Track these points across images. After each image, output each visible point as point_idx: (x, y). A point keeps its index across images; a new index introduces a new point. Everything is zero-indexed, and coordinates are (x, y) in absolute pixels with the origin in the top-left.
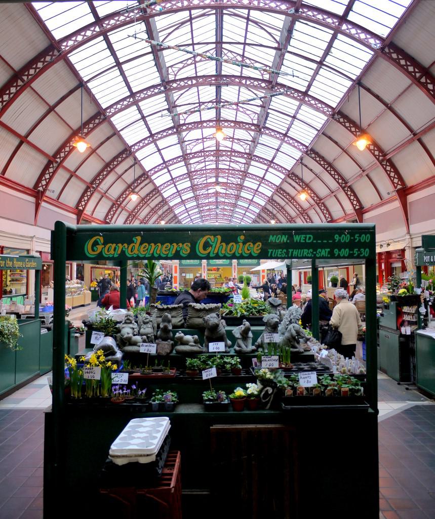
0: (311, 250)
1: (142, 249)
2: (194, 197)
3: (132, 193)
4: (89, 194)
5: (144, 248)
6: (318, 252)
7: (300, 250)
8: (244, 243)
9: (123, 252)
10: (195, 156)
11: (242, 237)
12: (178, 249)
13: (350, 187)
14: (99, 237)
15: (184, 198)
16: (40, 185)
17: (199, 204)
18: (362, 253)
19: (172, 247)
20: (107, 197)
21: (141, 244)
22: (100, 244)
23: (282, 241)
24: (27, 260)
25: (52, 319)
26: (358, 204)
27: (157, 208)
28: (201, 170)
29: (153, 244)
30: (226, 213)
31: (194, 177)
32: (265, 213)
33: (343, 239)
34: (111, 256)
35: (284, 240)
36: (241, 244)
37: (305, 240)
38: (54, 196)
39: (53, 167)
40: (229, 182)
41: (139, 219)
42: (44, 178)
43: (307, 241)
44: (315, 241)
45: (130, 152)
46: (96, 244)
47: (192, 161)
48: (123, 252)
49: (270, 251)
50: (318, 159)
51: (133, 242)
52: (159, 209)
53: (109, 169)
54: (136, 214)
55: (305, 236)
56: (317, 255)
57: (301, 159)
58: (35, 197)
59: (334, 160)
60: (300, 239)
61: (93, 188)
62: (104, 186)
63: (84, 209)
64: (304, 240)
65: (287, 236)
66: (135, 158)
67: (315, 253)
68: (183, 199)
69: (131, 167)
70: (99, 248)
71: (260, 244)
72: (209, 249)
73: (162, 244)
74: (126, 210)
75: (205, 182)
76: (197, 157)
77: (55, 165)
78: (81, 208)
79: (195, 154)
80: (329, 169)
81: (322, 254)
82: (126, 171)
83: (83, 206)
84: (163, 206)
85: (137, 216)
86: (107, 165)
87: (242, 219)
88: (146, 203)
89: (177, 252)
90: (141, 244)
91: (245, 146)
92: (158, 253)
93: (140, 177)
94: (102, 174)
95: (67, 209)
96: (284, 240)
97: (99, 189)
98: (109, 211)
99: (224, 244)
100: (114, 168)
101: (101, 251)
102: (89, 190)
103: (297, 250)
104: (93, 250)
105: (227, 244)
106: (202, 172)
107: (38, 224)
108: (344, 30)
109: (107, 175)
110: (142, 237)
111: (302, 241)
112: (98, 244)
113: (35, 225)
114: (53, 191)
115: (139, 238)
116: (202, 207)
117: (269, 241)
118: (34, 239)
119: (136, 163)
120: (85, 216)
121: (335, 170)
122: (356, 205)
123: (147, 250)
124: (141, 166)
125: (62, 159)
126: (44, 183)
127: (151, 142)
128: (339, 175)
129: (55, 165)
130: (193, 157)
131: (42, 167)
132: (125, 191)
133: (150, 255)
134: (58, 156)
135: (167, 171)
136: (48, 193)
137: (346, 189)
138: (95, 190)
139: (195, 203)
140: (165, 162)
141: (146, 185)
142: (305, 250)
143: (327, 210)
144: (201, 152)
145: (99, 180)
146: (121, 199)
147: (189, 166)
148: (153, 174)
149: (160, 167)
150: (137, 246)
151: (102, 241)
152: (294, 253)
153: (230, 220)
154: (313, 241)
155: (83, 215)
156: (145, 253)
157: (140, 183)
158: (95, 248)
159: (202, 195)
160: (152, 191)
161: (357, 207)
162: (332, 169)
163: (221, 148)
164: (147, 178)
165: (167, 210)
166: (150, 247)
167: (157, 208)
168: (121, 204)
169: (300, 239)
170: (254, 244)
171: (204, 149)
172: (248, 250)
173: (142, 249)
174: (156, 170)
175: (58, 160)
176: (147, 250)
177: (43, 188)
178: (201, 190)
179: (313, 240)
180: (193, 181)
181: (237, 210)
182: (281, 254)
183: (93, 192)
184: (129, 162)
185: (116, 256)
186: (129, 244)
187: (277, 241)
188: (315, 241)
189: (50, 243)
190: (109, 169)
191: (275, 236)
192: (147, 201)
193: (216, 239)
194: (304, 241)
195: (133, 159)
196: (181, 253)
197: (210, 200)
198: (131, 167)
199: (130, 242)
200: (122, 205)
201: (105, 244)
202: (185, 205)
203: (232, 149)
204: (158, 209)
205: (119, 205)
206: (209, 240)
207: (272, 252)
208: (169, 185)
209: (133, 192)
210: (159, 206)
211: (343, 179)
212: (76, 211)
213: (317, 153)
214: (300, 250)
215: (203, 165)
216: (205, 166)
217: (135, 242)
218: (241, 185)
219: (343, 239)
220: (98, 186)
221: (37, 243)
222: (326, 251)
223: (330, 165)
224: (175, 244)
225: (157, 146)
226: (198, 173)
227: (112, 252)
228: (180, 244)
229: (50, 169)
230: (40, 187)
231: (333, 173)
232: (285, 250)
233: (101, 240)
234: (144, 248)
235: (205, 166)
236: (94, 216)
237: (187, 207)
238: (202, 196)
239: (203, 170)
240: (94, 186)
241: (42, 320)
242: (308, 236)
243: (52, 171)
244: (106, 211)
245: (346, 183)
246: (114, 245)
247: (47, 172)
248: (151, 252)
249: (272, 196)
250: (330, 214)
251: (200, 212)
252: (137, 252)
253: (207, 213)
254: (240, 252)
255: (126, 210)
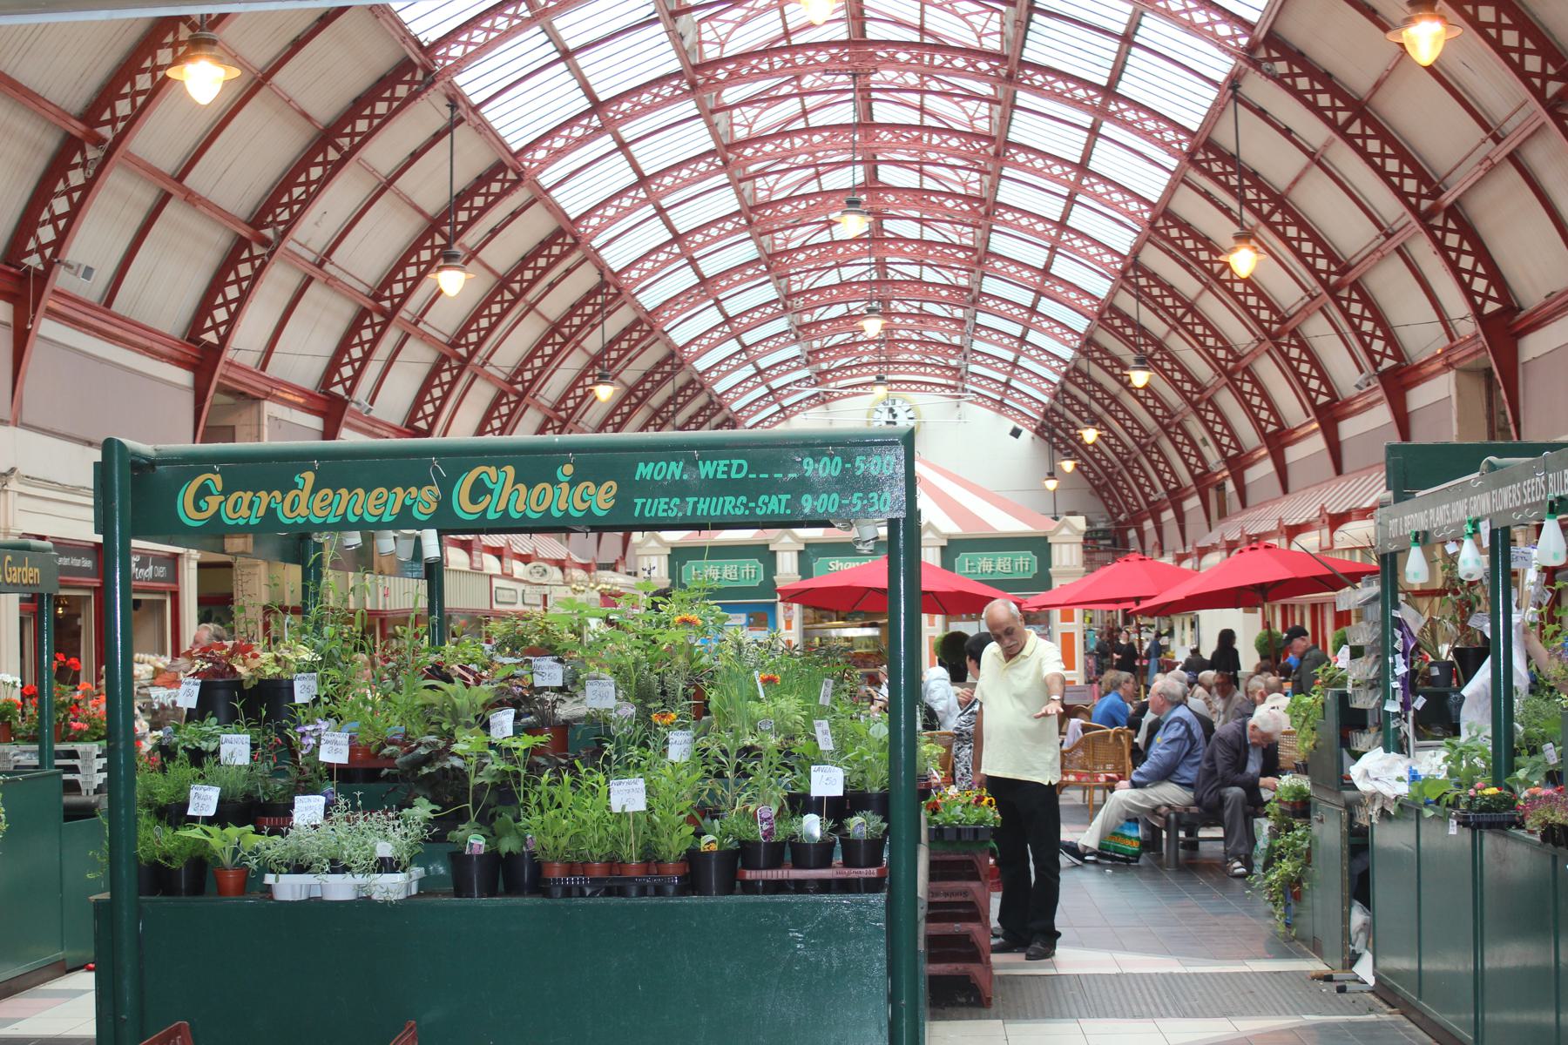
0: (743, 499)
1: (317, 504)
2: (757, 261)
3: (441, 262)
4: (245, 270)
5: (323, 500)
6: (760, 503)
7: (708, 499)
8: (573, 483)
9: (271, 512)
10: (744, 71)
11: (569, 469)
12: (408, 502)
13: (1453, 211)
14: (209, 475)
15: (710, 267)
16: (32, 245)
17: (789, 296)
18: (872, 505)
19: (392, 496)
20: (330, 281)
21: (315, 490)
22: (214, 492)
23: (669, 477)
24: (9, 558)
25: (105, 775)
26: (1493, 293)
27: (577, 321)
28: (782, 134)
29: (344, 491)
30: (936, 336)
31: (752, 169)
32: (1114, 330)
33: (824, 469)
34: (242, 522)
35: (673, 475)
36: (565, 487)
37: (728, 473)
38: (93, 290)
39: (84, 165)
40: (929, 184)
41: (489, 378)
42: (45, 215)
43: (734, 475)
44: (754, 476)
45: (428, 72)
46: (204, 491)
47: (731, 95)
48: (271, 512)
49: (639, 501)
50: (1303, 83)
51: (295, 486)
52: (590, 323)
53: (333, 155)
54: (471, 354)
55: (727, 462)
56: (758, 510)
57: (1234, 81)
58: (8, 301)
59: (1377, 86)
60: (716, 471)
61: (265, 242)
62: (313, 230)
63: (224, 340)
64: (723, 472)
65: (681, 464)
66: (455, 99)
67: (752, 505)
68: (708, 273)
69: (437, 137)
70: (213, 502)
71: (613, 484)
72: (485, 501)
73: (368, 490)
74: (425, 338)
75: (812, 187)
76: (751, 78)
77: (93, 153)
78: (211, 337)
79: (741, 65)
80: (1355, 129)
81: (771, 507)
82: (415, 156)
83: (222, 329)
84: (604, 311)
85: (476, 360)
86: (326, 136)
87: (1014, 364)
88: (518, 297)
89: (406, 510)
90: (315, 490)
91: (978, 21)
92: (358, 511)
93: (483, 180)
94: (302, 179)
95: (148, 343)
96: (673, 475)
97: (289, 244)
98: (344, 346)
99: (522, 487)
100: (355, 149)
101: (218, 511)
102: (246, 255)
103: (708, 499)
104: (198, 509)
105: (530, 486)
106: (787, 144)
107: (27, 417)
108: (591, 118)
109: (324, 182)
110: (316, 472)
111: (720, 476)
112: (212, 494)
113: (17, 422)
114: (88, 272)
115: (310, 476)
116: (811, 310)
117: (637, 478)
118: (13, 485)
119: (461, 120)
120: (232, 374)
121: (1384, 135)
122: (1486, 296)
123: (331, 504)
124: (484, 129)
125: (120, 125)
126: (46, 234)
127: (527, 23)
128: (1403, 155)
129: (93, 153)
130: (734, 78)
131: (39, 165)
132: (416, 247)
133: (338, 519)
134: (107, 116)
135: (614, 145)
136: (62, 279)
137: (1438, 221)
138: (271, 254)
139: (769, 292)
140: (597, 106)
141: (514, 215)
142: (728, 499)
143: (1379, 319)
144: (768, 52)
145: (289, 205)
146: (398, 289)
147: (717, 117)
148: (544, 164)
149: (578, 132)
150: (305, 495)
151: (220, 487)
152: (700, 506)
153: (957, 369)
154: (747, 475)
155: (220, 369)
156: (324, 513)
157: (483, 211)
158: (202, 503)
159: (802, 248)
160: (545, 244)
161: (1490, 307)
162: (1369, 131)
163: (874, 31)
164: (516, 184)
165: (628, 330)
166: (338, 497)
167: (577, 321)
168: (396, 308)
169: (716, 471)
170: (598, 484)
171: (787, 34)
172: (583, 501)
173: (317, 504)
174: (559, 143)
175: (106, 132)
176: (331, 504)
177: (43, 256)
178: (795, 227)
179: (748, 473)
180: (747, 186)
181: (982, 319)
182: (664, 511)
183: (264, 265)
184: (427, 114)
185: (254, 521)
186: (284, 492)
187: (656, 478)
188: (751, 476)
189: (91, 501)
190: (333, 155)
191: (651, 465)
192: (524, 291)
193: (502, 475)
194: (725, 476)
195: (442, 103)
196: (415, 513)
197: (848, 273)
198: (437, 137)
199: (287, 486)
200: (403, 314)
201: (226, 492)
202: (718, 302)
203: (922, 30)
204: (580, 328)
205: (389, 316)
206: (484, 476)
207: (644, 505)
208: (630, 210)
209: (447, 257)
210: (589, 310)
211: (1421, 175)
212: (192, 353)
213: (1296, 57)
214: (715, 499)
215: (793, 106)
216: (805, 113)
217: (300, 487)
218: (982, 200)
219: (824, 469)
220: (284, 234)
221: (24, 500)
222: (780, 501)
223: (1360, 108)
224: (399, 490)
225: (553, 37)
226: (769, 148)
227: (244, 512)
228: (413, 490)
229: (71, 174)
230: (30, 253)
231: (1374, 146)
232: (676, 501)
233: (216, 482)
234: (323, 500)
235: (805, 113)
236: (274, 370)
237: (733, 308)
238: (801, 257)
239: (790, 134)
240: (269, 233)
241: (67, 777)
242: (735, 462)
243: (81, 181)
244: (328, 346)
245: (1436, 193)
246: (250, 494)
247: (60, 187)
248: (341, 511)
249: (1136, 250)
250: (1390, 338)
251: (802, 331)
252: (304, 512)
253: (839, 338)
254: (563, 506)
255: (425, 338)
